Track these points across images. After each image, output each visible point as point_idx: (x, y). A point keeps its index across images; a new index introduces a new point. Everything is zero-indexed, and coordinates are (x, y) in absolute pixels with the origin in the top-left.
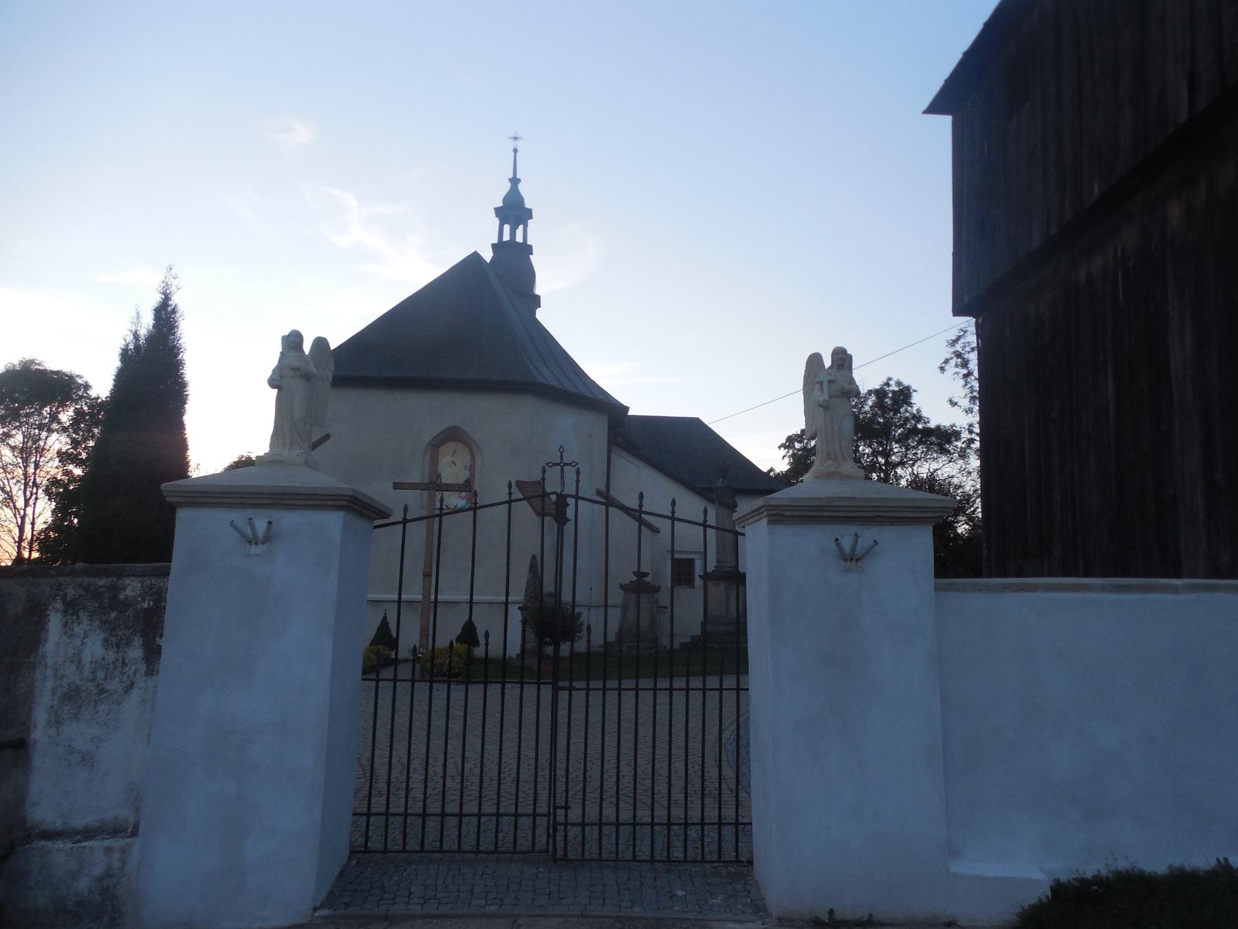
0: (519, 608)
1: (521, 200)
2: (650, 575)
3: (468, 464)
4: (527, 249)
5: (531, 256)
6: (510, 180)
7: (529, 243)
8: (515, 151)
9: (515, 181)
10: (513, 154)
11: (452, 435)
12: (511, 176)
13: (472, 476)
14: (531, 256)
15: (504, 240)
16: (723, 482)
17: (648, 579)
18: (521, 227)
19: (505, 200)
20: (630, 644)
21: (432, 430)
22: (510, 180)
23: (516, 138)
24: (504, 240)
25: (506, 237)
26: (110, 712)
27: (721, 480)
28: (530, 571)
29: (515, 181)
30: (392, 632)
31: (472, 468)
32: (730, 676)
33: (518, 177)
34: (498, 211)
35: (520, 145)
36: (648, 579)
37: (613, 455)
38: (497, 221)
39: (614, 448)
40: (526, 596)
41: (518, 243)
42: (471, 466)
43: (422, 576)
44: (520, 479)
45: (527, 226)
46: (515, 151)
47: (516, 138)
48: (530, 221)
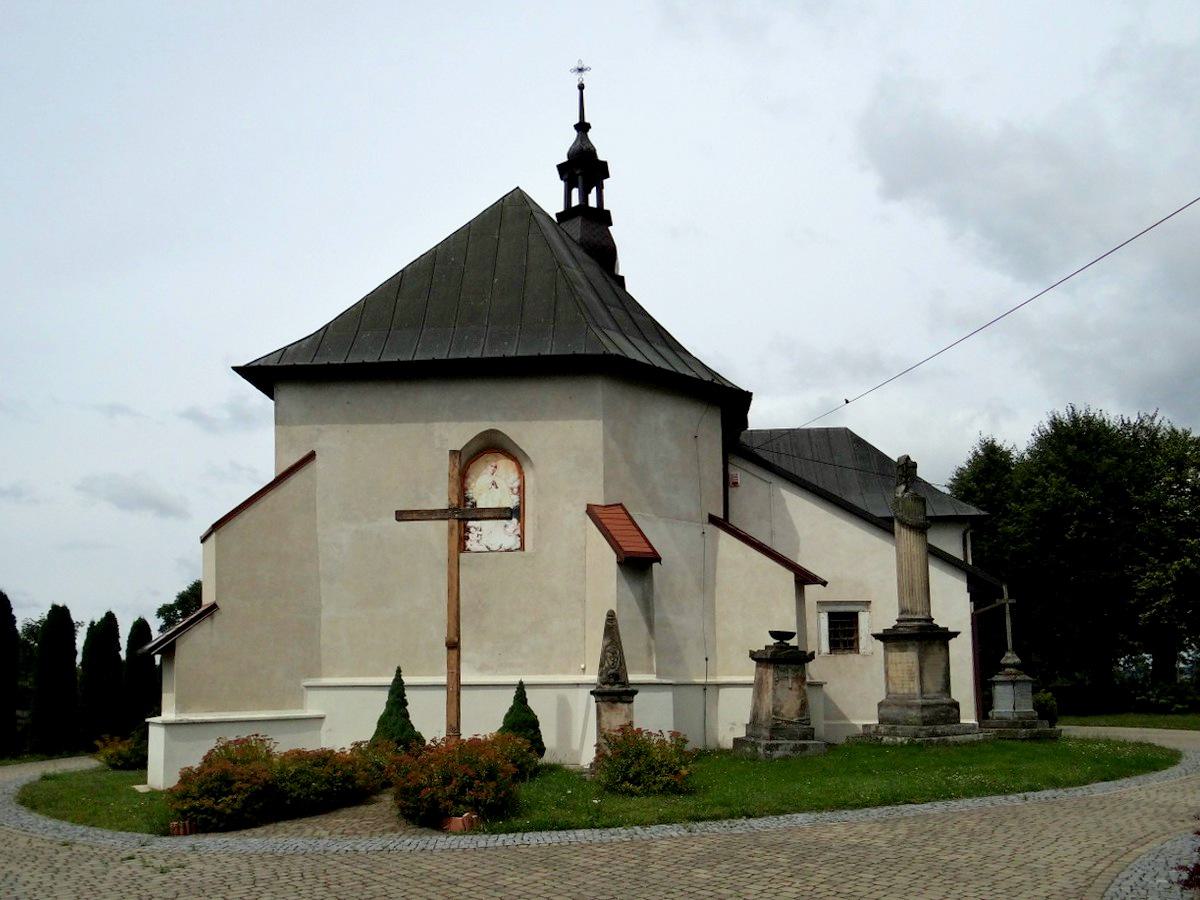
0: (592, 693)
1: (592, 152)
2: (796, 637)
3: (516, 484)
4: (603, 217)
5: (610, 228)
6: (577, 127)
7: (605, 208)
8: (581, 87)
9: (583, 127)
10: (578, 91)
11: (492, 446)
12: (577, 121)
13: (522, 501)
14: (610, 228)
15: (573, 205)
16: (905, 491)
17: (793, 642)
18: (594, 190)
19: (569, 155)
20: (769, 742)
21: (461, 434)
22: (577, 127)
23: (581, 70)
24: (573, 205)
25: (575, 201)
26: (183, 867)
27: (903, 487)
28: (605, 636)
29: (583, 127)
30: (120, 640)
31: (521, 490)
32: (1132, 714)
33: (587, 120)
34: (563, 169)
35: (586, 78)
36: (793, 642)
37: (731, 467)
38: (561, 185)
39: (743, 473)
40: (600, 675)
41: (592, 208)
42: (519, 488)
43: (446, 648)
44: (593, 503)
45: (603, 187)
46: (581, 87)
47: (581, 70)
48: (605, 181)
